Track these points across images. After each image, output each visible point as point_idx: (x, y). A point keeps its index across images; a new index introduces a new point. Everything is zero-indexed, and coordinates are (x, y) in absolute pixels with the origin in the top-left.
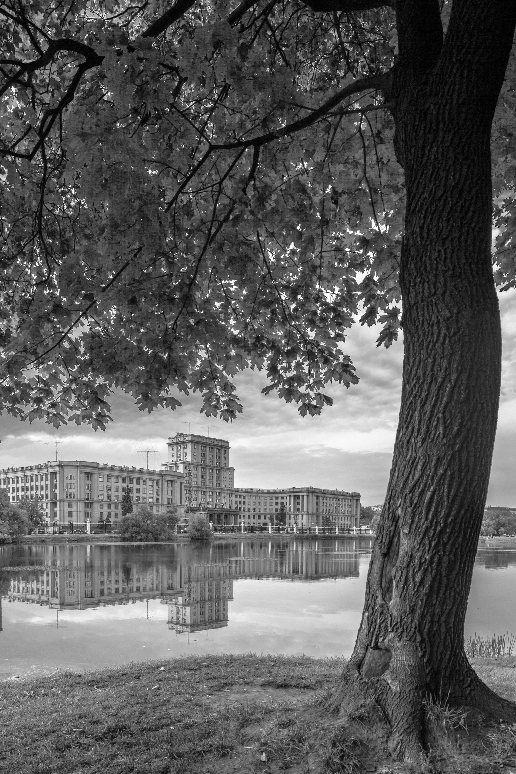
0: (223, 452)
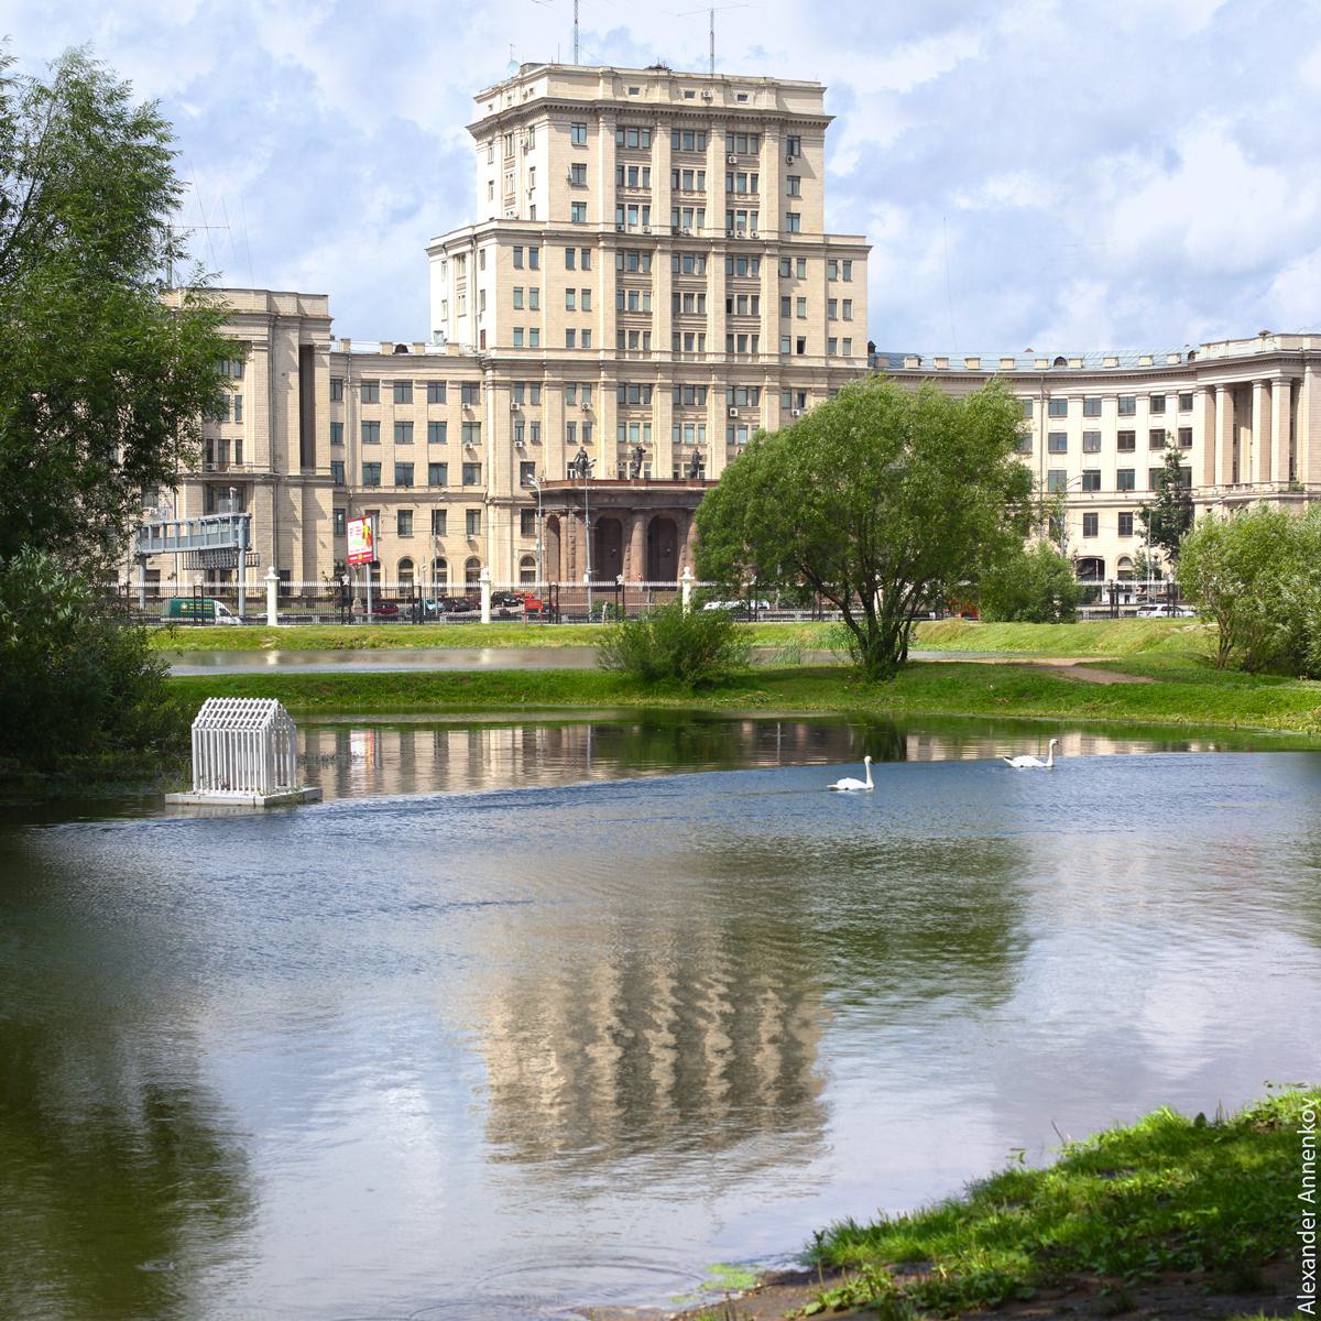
0: (769, 153)
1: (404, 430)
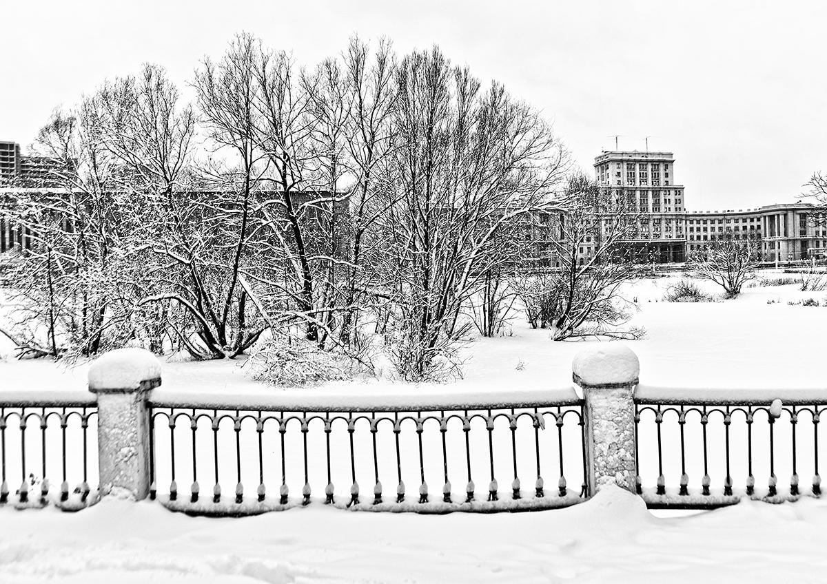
1: (698, 229)
